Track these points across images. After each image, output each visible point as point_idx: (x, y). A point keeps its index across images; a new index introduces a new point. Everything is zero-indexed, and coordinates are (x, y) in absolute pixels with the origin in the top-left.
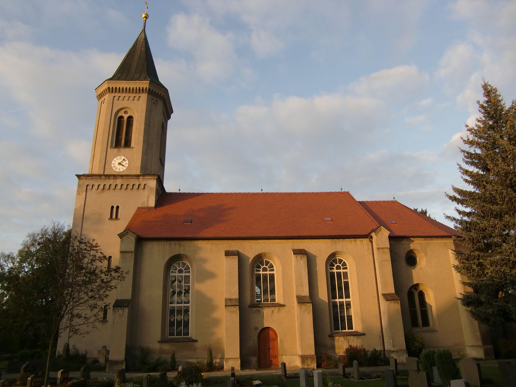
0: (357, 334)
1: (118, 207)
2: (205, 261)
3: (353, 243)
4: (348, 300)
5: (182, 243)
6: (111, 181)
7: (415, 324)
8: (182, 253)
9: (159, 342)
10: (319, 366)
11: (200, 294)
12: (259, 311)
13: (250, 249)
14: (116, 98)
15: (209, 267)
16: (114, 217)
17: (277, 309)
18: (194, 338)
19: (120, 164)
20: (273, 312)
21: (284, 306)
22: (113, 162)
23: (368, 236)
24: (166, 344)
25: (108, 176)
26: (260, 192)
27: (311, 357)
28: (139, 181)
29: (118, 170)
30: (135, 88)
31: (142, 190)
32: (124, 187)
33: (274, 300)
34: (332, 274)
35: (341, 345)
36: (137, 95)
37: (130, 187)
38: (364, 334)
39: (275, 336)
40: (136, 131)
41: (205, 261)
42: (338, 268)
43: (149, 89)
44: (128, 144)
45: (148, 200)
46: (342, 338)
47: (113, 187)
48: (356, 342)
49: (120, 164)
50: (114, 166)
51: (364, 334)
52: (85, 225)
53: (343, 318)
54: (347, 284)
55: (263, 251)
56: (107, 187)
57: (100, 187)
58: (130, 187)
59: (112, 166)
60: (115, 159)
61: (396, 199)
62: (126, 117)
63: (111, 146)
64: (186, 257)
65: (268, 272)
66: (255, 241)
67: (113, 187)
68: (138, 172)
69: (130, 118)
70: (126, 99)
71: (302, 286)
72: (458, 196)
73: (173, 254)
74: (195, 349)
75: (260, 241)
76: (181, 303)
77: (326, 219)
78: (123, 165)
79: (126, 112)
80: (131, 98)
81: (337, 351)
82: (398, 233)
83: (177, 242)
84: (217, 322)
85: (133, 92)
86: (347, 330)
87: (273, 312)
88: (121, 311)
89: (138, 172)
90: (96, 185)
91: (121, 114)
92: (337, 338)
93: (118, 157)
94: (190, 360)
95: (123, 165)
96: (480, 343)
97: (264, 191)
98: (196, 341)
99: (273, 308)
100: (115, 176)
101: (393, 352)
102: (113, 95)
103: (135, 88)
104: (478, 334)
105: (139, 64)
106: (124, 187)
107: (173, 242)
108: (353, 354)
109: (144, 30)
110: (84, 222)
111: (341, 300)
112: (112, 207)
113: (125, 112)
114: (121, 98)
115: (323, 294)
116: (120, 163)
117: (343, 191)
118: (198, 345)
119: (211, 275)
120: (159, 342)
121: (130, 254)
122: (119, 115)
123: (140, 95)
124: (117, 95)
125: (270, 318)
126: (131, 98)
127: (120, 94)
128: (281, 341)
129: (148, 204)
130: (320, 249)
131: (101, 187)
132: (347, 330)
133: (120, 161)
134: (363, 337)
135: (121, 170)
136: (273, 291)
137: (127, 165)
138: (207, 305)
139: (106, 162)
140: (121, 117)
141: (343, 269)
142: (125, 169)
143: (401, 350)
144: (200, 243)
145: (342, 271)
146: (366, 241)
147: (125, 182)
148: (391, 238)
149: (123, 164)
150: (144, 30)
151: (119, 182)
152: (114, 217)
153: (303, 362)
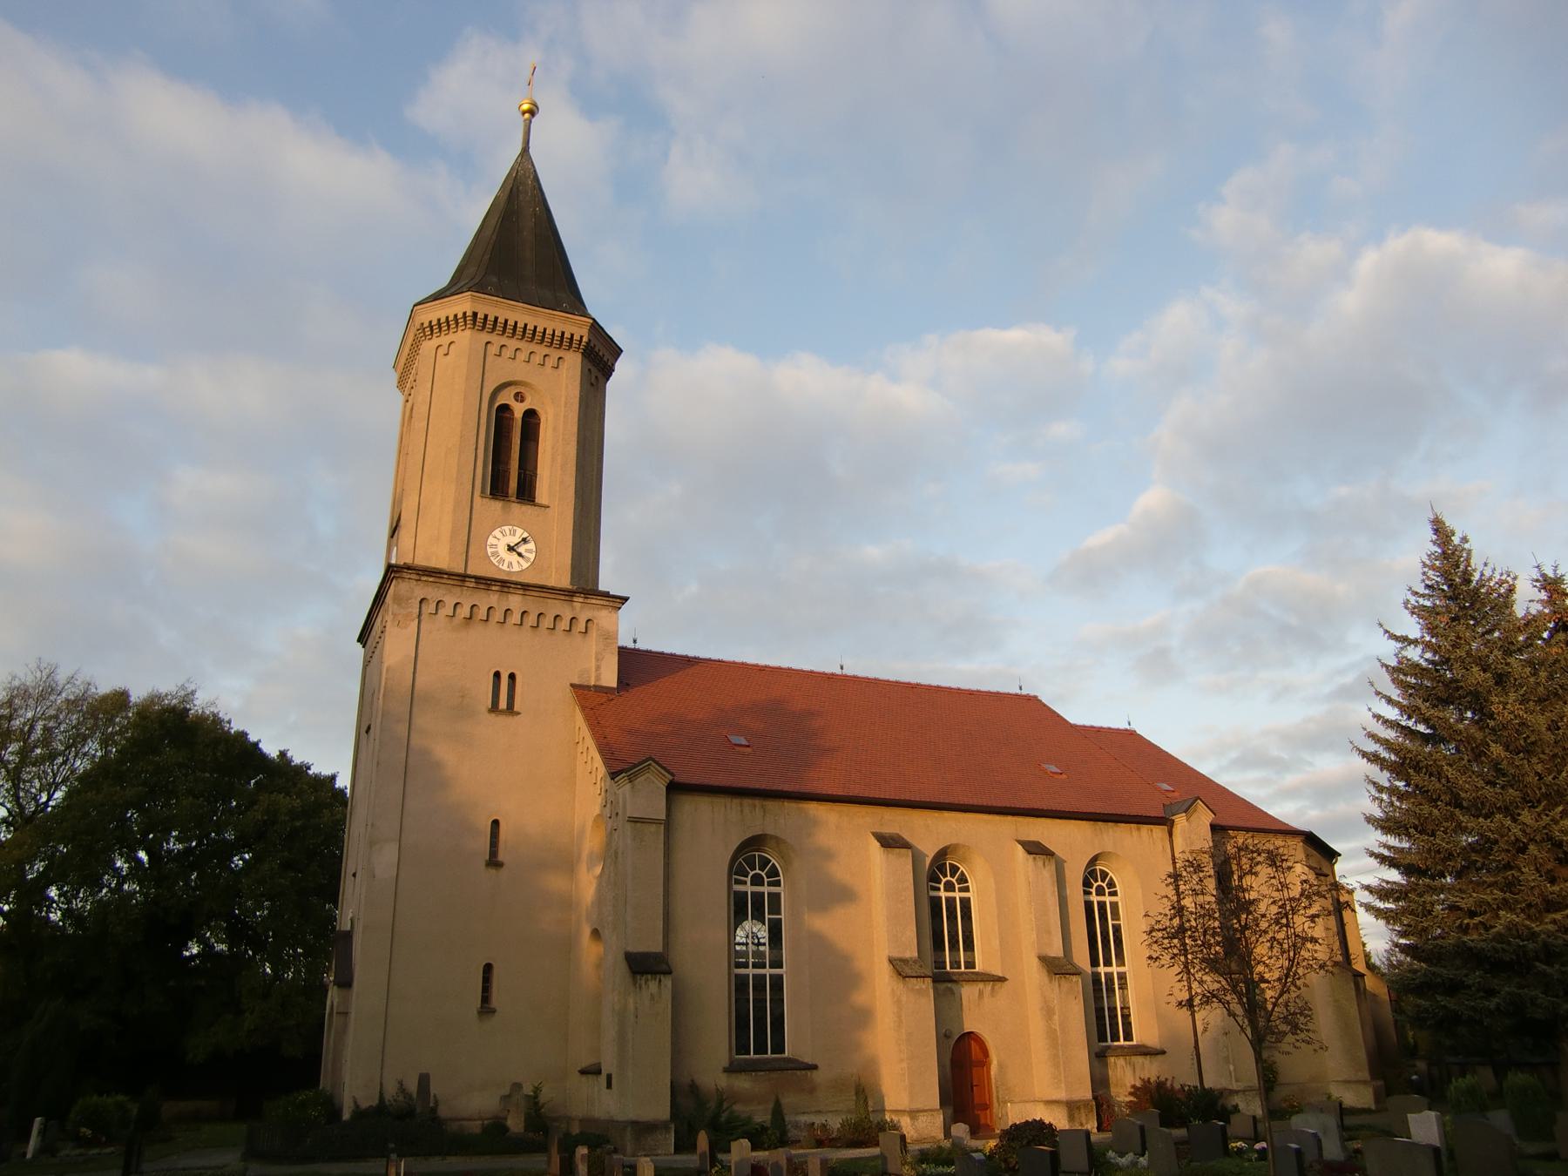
0: (1144, 1051)
1: (512, 677)
2: (828, 855)
3: (1135, 833)
4: (1121, 969)
5: (772, 805)
6: (493, 598)
7: (1102, 1038)
8: (770, 831)
9: (726, 1070)
10: (1099, 1129)
11: (820, 942)
12: (952, 992)
13: (931, 832)
14: (493, 349)
15: (840, 871)
16: (503, 704)
17: (989, 987)
18: (808, 1060)
19: (511, 549)
20: (981, 994)
21: (1002, 980)
22: (491, 540)
23: (1165, 821)
24: (743, 1076)
25: (485, 583)
26: (839, 672)
27: (1086, 1103)
28: (573, 608)
29: (505, 567)
30: (549, 332)
31: (579, 638)
32: (531, 619)
33: (970, 964)
34: (935, 903)
35: (1125, 1077)
36: (555, 354)
37: (547, 622)
38: (1163, 1053)
39: (980, 1056)
40: (553, 460)
41: (828, 855)
42: (949, 887)
43: (588, 343)
44: (526, 493)
45: (598, 668)
46: (1121, 1061)
47: (498, 615)
48: (1150, 1070)
49: (511, 549)
50: (495, 554)
51: (1163, 1053)
52: (419, 721)
53: (1113, 1010)
54: (1117, 929)
55: (954, 841)
56: (482, 613)
57: (458, 610)
58: (547, 622)
59: (489, 550)
60: (497, 533)
61: (1134, 727)
62: (519, 410)
63: (483, 491)
64: (778, 840)
65: (766, 889)
66: (936, 814)
67: (498, 615)
68: (565, 582)
69: (531, 415)
70: (522, 356)
71: (1049, 932)
72: (1384, 754)
73: (749, 835)
74: (812, 1090)
75: (946, 814)
76: (746, 965)
77: (735, 739)
78: (520, 555)
79: (519, 397)
80: (537, 359)
81: (1113, 1091)
82: (682, 778)
83: (757, 802)
84: (863, 1017)
85: (542, 341)
86: (770, 1055)
87: (981, 994)
88: (653, 985)
89: (565, 582)
90: (450, 601)
91: (506, 398)
92: (1112, 1059)
93: (506, 528)
94: (819, 1120)
95: (520, 555)
96: (1365, 1075)
97: (848, 671)
98: (815, 1067)
99: (981, 985)
100: (505, 585)
101: (1237, 1092)
102: (485, 337)
103: (549, 332)
104: (1362, 1055)
105: (519, 254)
106: (531, 619)
107: (747, 802)
108: (1156, 1097)
109: (525, 150)
110: (415, 709)
111: (1108, 969)
112: (497, 675)
113: (517, 394)
114: (507, 353)
115: (1081, 957)
116: (511, 545)
117: (1024, 692)
118: (818, 1077)
119: (843, 895)
120: (726, 1070)
121: (653, 828)
122: (500, 401)
123: (561, 353)
124: (497, 340)
125: (979, 1012)
126: (537, 359)
127: (504, 340)
128: (1001, 1066)
129: (598, 678)
130: (1074, 841)
131: (464, 611)
132: (770, 1055)
133: (513, 541)
134: (1160, 1057)
135: (516, 568)
136: (969, 946)
137: (532, 556)
138: (840, 974)
139: (470, 539)
140: (505, 408)
141: (770, 884)
142: (525, 565)
143: (1251, 1089)
144: (813, 808)
145: (766, 889)
146: (1159, 832)
147: (533, 605)
148: (1215, 828)
149: (521, 549)
150: (525, 150)
151: (515, 601)
152: (503, 704)
153: (1071, 1118)
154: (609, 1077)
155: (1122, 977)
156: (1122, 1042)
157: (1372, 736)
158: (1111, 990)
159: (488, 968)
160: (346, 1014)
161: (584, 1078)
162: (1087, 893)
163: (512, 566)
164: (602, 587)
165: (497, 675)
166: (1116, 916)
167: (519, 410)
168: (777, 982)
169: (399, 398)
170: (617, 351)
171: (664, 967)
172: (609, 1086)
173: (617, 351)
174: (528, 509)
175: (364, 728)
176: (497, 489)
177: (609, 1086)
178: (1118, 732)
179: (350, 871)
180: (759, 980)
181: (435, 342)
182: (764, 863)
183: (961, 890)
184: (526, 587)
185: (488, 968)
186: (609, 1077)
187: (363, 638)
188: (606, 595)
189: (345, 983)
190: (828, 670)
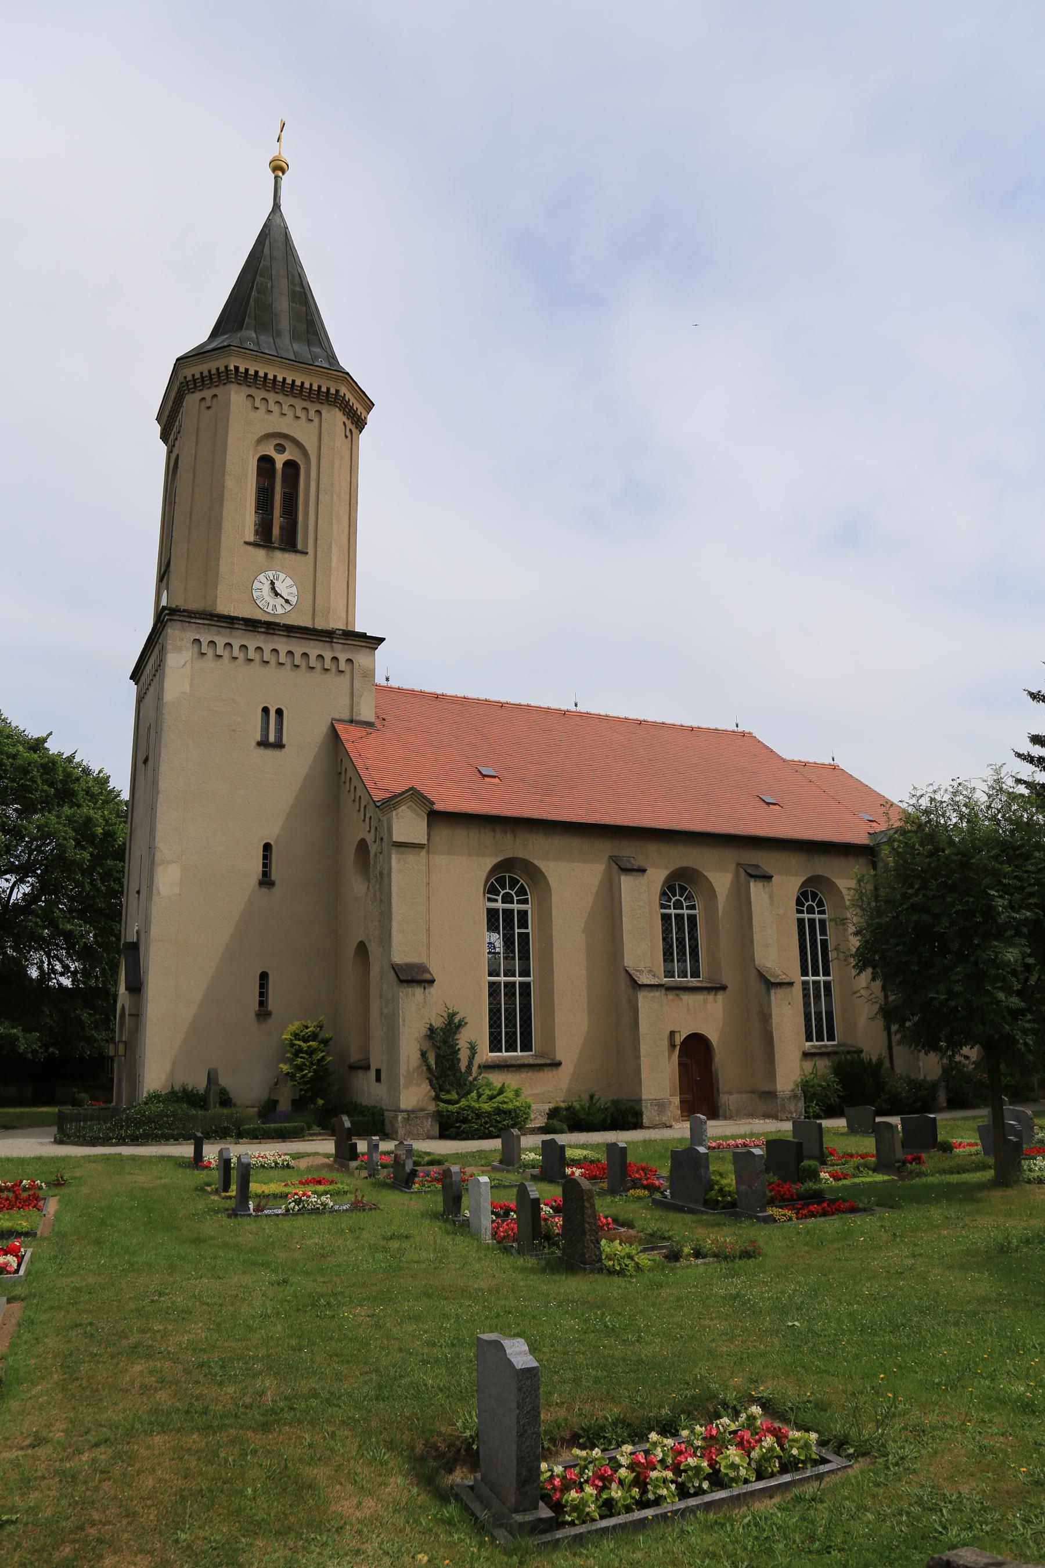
1: (279, 712)
26: (573, 709)
53: (818, 1014)
54: (824, 943)
62: (280, 460)
90: (328, 655)
109: (276, 206)
112: (266, 710)
135: (280, 611)
145: (817, 916)
150: (276, 206)
151: (283, 645)
154: (378, 1072)
155: (827, 985)
156: (825, 1043)
157: (1030, 759)
158: (817, 997)
159: (264, 976)
160: (137, 1016)
161: (667, 1034)
162: (799, 911)
163: (273, 608)
164: (358, 629)
165: (266, 710)
166: (523, 924)
167: (280, 460)
168: (525, 987)
169: (163, 448)
170: (369, 405)
171: (427, 977)
172: (378, 1079)
173: (369, 405)
174: (290, 557)
175: (140, 761)
176: (264, 538)
177: (378, 1079)
178: (823, 766)
179: (134, 887)
180: (816, 973)
181: (198, 395)
182: (514, 882)
183: (820, 913)
184: (291, 631)
185: (264, 976)
186: (378, 1072)
187: (135, 676)
188: (363, 636)
189: (136, 988)
190: (564, 708)
